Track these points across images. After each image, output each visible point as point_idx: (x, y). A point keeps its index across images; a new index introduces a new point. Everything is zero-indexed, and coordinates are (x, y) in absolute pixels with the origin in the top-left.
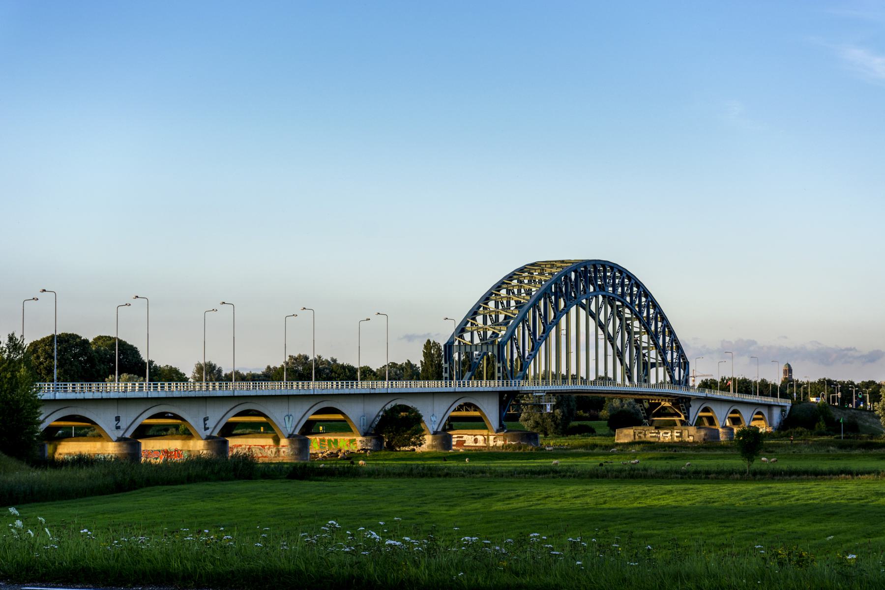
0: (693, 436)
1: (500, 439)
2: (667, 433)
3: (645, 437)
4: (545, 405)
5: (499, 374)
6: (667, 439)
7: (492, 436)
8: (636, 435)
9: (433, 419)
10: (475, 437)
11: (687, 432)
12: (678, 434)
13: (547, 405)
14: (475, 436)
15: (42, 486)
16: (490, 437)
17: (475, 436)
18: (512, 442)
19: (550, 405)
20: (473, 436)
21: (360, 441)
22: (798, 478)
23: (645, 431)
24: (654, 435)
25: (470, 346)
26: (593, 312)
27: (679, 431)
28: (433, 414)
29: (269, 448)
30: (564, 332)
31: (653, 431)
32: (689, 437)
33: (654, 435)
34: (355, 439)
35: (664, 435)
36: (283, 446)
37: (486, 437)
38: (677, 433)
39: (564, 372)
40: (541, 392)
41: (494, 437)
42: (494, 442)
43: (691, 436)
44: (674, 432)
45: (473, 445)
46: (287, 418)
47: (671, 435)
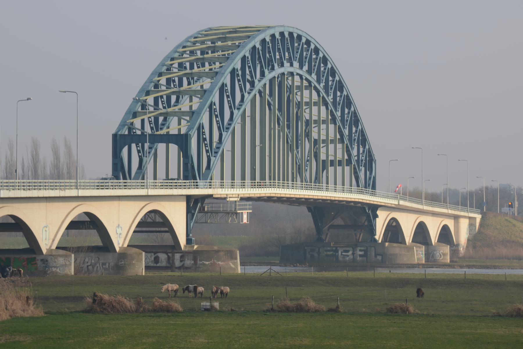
0: (382, 255)
4: (242, 213)
6: (347, 258)
8: (307, 254)
9: (119, 231)
10: (156, 255)
11: (373, 249)
13: (244, 214)
14: (155, 253)
15: (223, 265)
16: (176, 254)
17: (155, 253)
19: (246, 214)
20: (153, 254)
26: (200, 104)
27: (362, 249)
28: (119, 225)
30: (361, 122)
32: (376, 256)
33: (331, 253)
37: (170, 255)
38: (360, 250)
39: (339, 169)
40: (234, 196)
42: (181, 261)
43: (379, 255)
45: (152, 265)
47: (353, 254)
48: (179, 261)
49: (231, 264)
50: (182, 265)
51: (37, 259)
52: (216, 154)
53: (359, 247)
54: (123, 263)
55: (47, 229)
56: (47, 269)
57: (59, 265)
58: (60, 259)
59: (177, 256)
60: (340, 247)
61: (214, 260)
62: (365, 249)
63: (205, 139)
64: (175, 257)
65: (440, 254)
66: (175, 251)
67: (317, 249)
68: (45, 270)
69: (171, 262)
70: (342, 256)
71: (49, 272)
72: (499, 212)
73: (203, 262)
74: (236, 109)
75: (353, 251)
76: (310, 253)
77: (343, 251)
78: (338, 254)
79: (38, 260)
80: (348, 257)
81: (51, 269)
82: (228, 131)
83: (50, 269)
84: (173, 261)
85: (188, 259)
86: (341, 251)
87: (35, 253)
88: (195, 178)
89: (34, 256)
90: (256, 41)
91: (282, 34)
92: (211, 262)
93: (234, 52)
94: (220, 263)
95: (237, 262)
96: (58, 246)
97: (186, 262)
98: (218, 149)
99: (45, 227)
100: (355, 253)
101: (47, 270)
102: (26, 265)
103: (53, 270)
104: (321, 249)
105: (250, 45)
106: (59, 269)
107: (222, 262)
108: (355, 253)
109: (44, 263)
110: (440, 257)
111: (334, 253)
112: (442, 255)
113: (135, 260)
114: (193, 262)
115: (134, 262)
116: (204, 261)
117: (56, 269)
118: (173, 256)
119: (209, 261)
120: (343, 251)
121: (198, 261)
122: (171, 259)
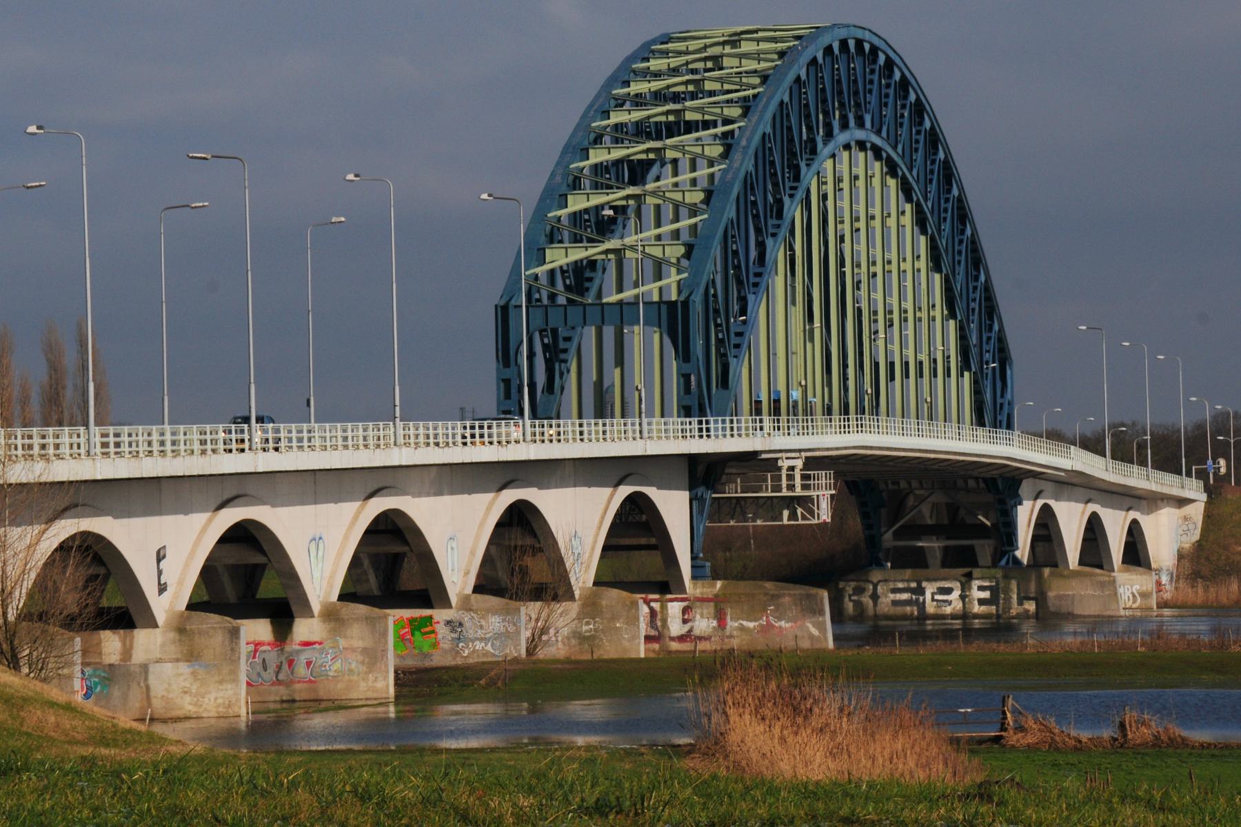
1: (705, 611)
2: (948, 591)
3: (875, 604)
5: (508, 402)
7: (675, 604)
12: (986, 595)
16: (670, 604)
18: (745, 623)
21: (448, 623)
22: (221, 687)
23: (875, 586)
24: (905, 596)
25: (563, 308)
27: (987, 584)
29: (256, 651)
31: (900, 585)
33: (905, 596)
34: (431, 617)
35: (937, 597)
36: (307, 644)
38: (981, 588)
41: (685, 604)
42: (685, 621)
44: (970, 588)
46: (313, 545)
47: (963, 597)
48: (679, 620)
49: (810, 625)
50: (688, 632)
51: (436, 621)
52: (736, 350)
53: (978, 579)
54: (591, 626)
55: (454, 545)
56: (461, 645)
57: (491, 634)
58: (493, 620)
59: (675, 608)
60: (928, 580)
61: (767, 617)
62: (994, 584)
63: (716, 311)
64: (670, 611)
65: (1133, 594)
66: (669, 596)
67: (871, 587)
68: (458, 647)
69: (659, 624)
70: (935, 603)
71: (467, 652)
72: (1233, 484)
73: (741, 622)
74: (770, 237)
75: (963, 590)
76: (853, 598)
77: (936, 591)
78: (924, 600)
79: (438, 623)
80: (950, 605)
81: (471, 644)
82: (759, 291)
83: (470, 646)
84: (664, 621)
85: (702, 617)
86: (932, 591)
87: (429, 605)
88: (86, 424)
89: (426, 612)
90: (801, 63)
91: (844, 43)
92: (761, 622)
93: (759, 93)
94: (783, 623)
95: (824, 622)
96: (345, 592)
97: (697, 623)
98: (568, 343)
99: (311, 541)
100: (966, 596)
101: (463, 647)
102: (408, 637)
103: (477, 648)
104: (879, 587)
105: (791, 77)
106: (492, 646)
107: (787, 622)
108: (966, 596)
109: (453, 631)
110: (1134, 602)
111: (914, 597)
112: (1137, 595)
113: (621, 621)
114: (715, 623)
115: (618, 625)
116: (743, 620)
117: (483, 644)
118: (664, 608)
119: (755, 621)
120: (936, 591)
121: (729, 621)
122: (659, 617)
